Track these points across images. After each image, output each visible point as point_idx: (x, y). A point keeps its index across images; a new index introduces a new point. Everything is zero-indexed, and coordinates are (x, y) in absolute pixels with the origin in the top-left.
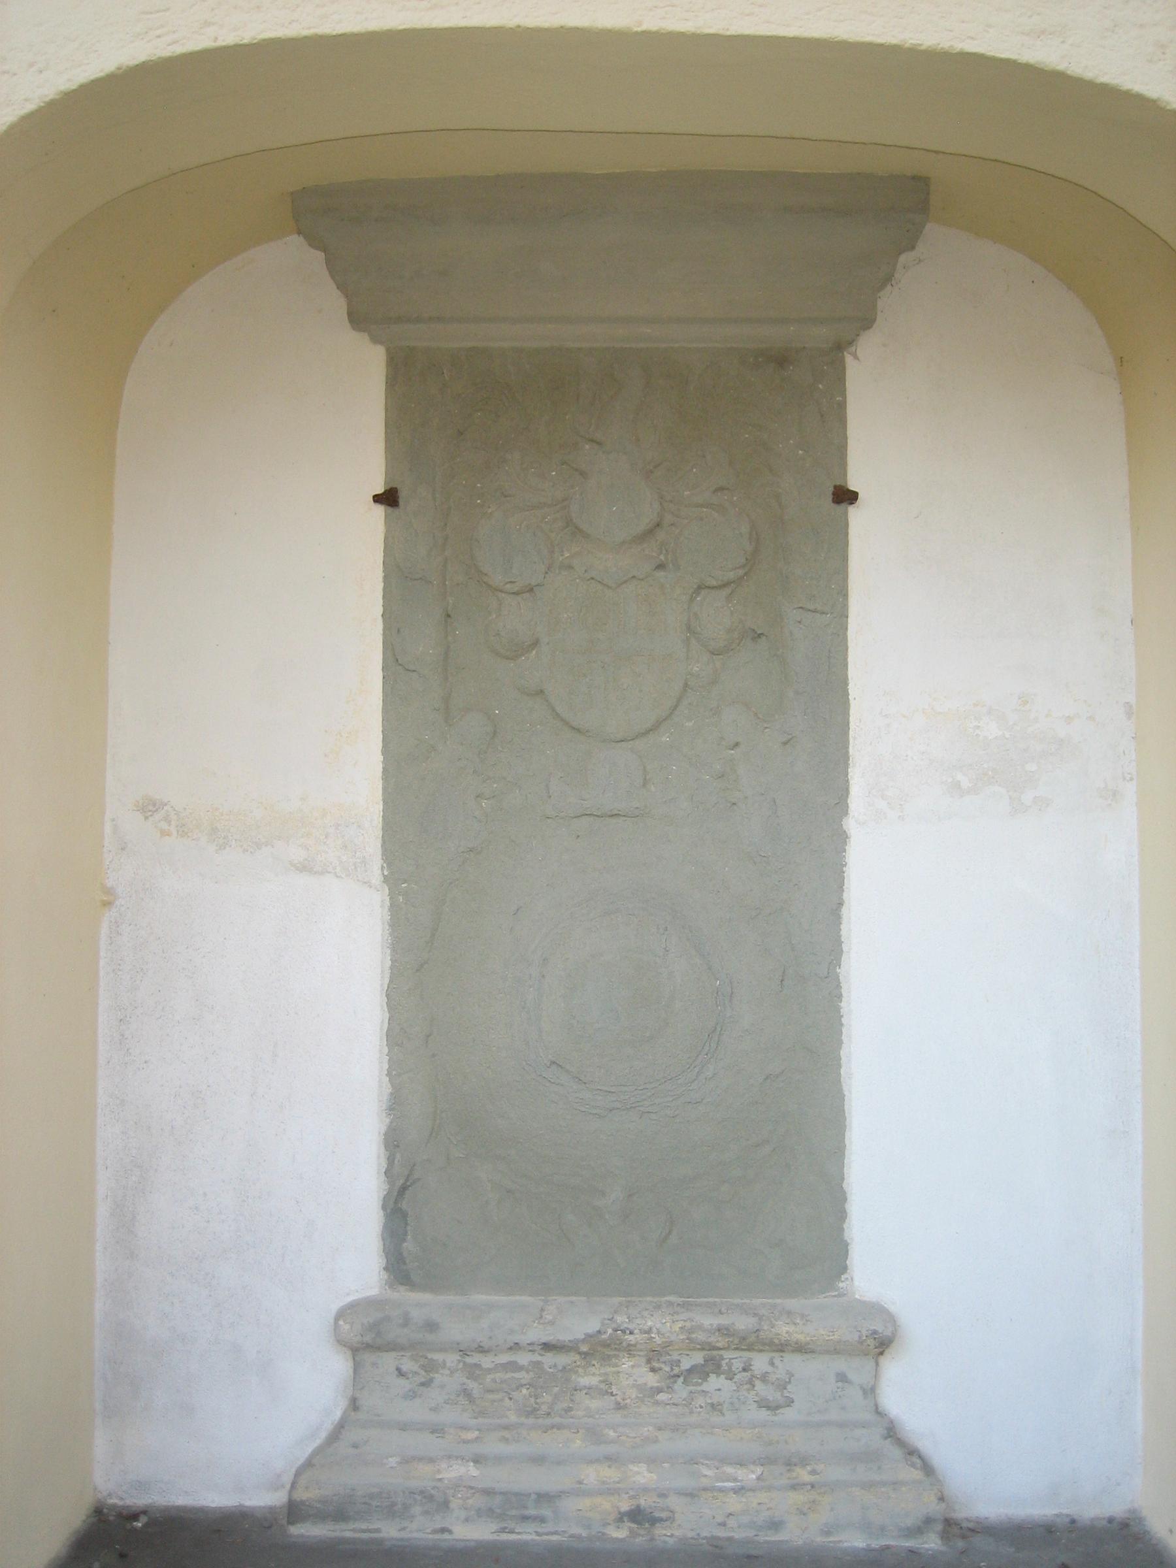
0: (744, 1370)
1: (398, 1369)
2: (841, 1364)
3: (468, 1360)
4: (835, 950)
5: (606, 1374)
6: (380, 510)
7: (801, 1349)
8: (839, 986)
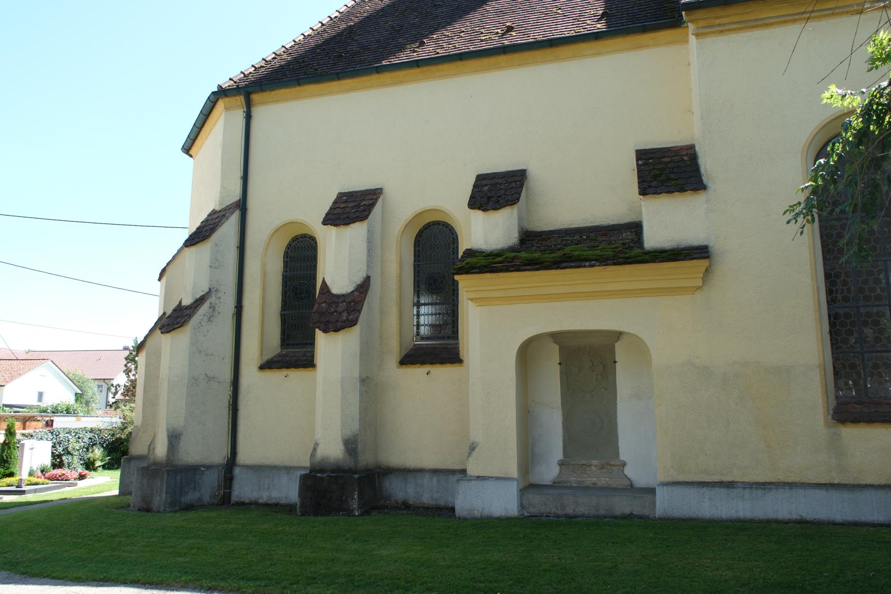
4: (616, 417)
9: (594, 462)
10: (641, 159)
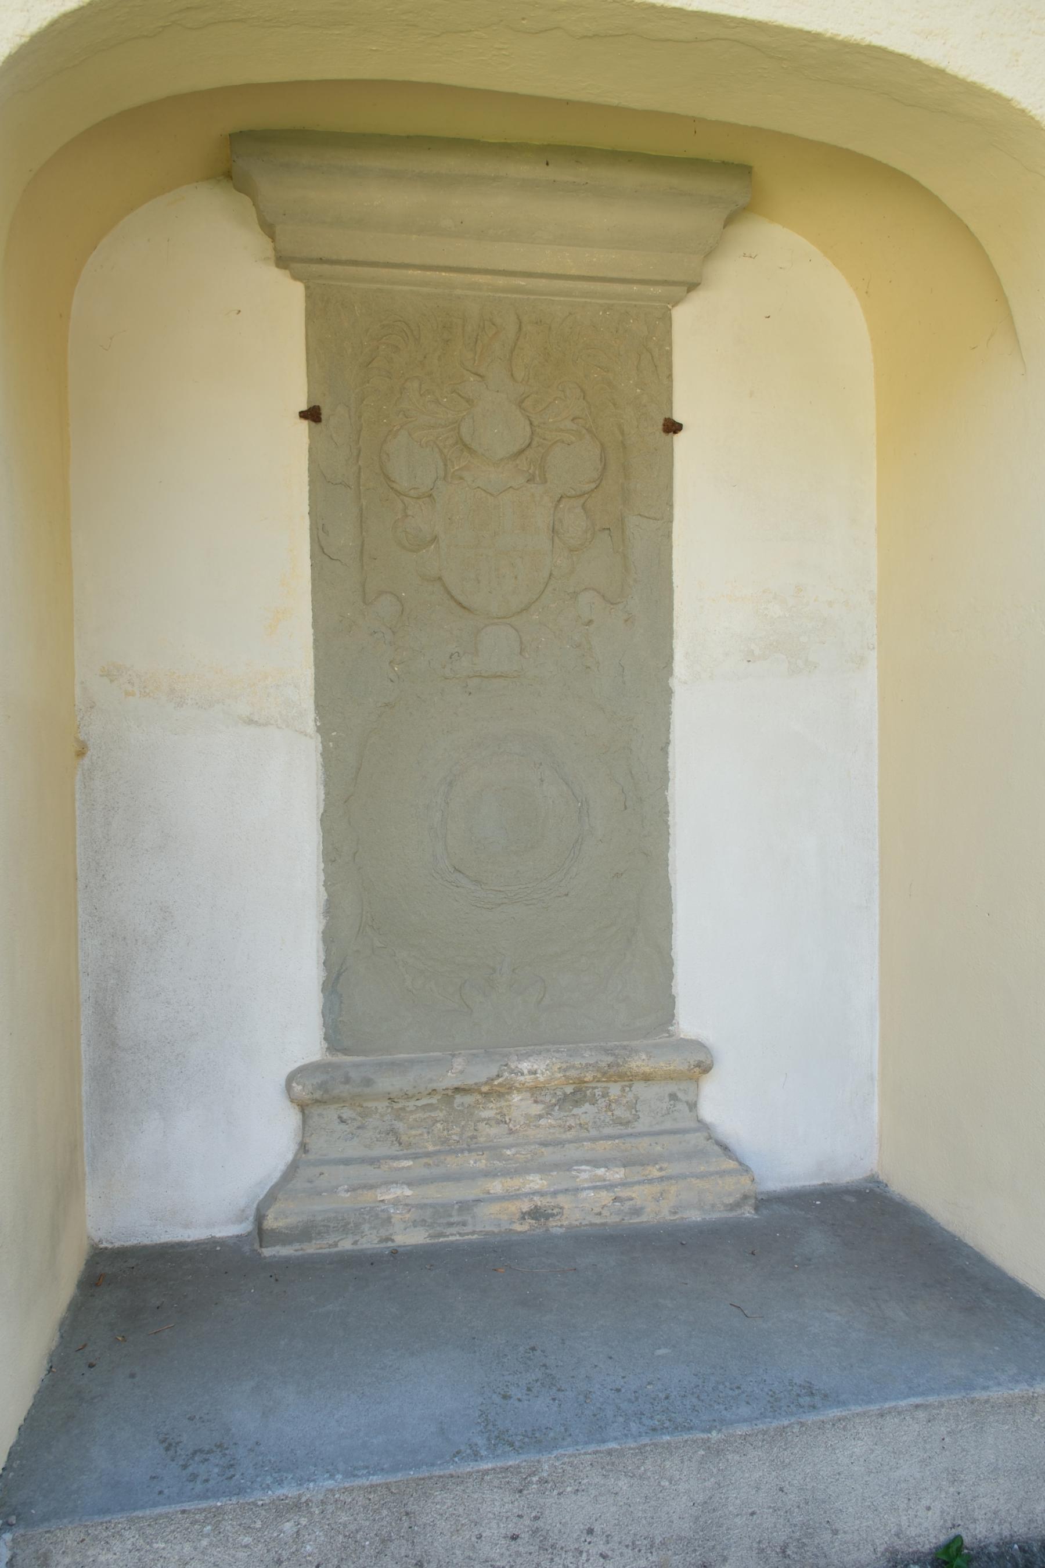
0: (603, 1096)
1: (340, 1117)
2: (672, 1087)
3: (396, 1106)
4: (663, 778)
5: (501, 1108)
6: (305, 424)
7: (647, 1078)
8: (667, 805)
9: (535, 1067)
10: (667, 351)
